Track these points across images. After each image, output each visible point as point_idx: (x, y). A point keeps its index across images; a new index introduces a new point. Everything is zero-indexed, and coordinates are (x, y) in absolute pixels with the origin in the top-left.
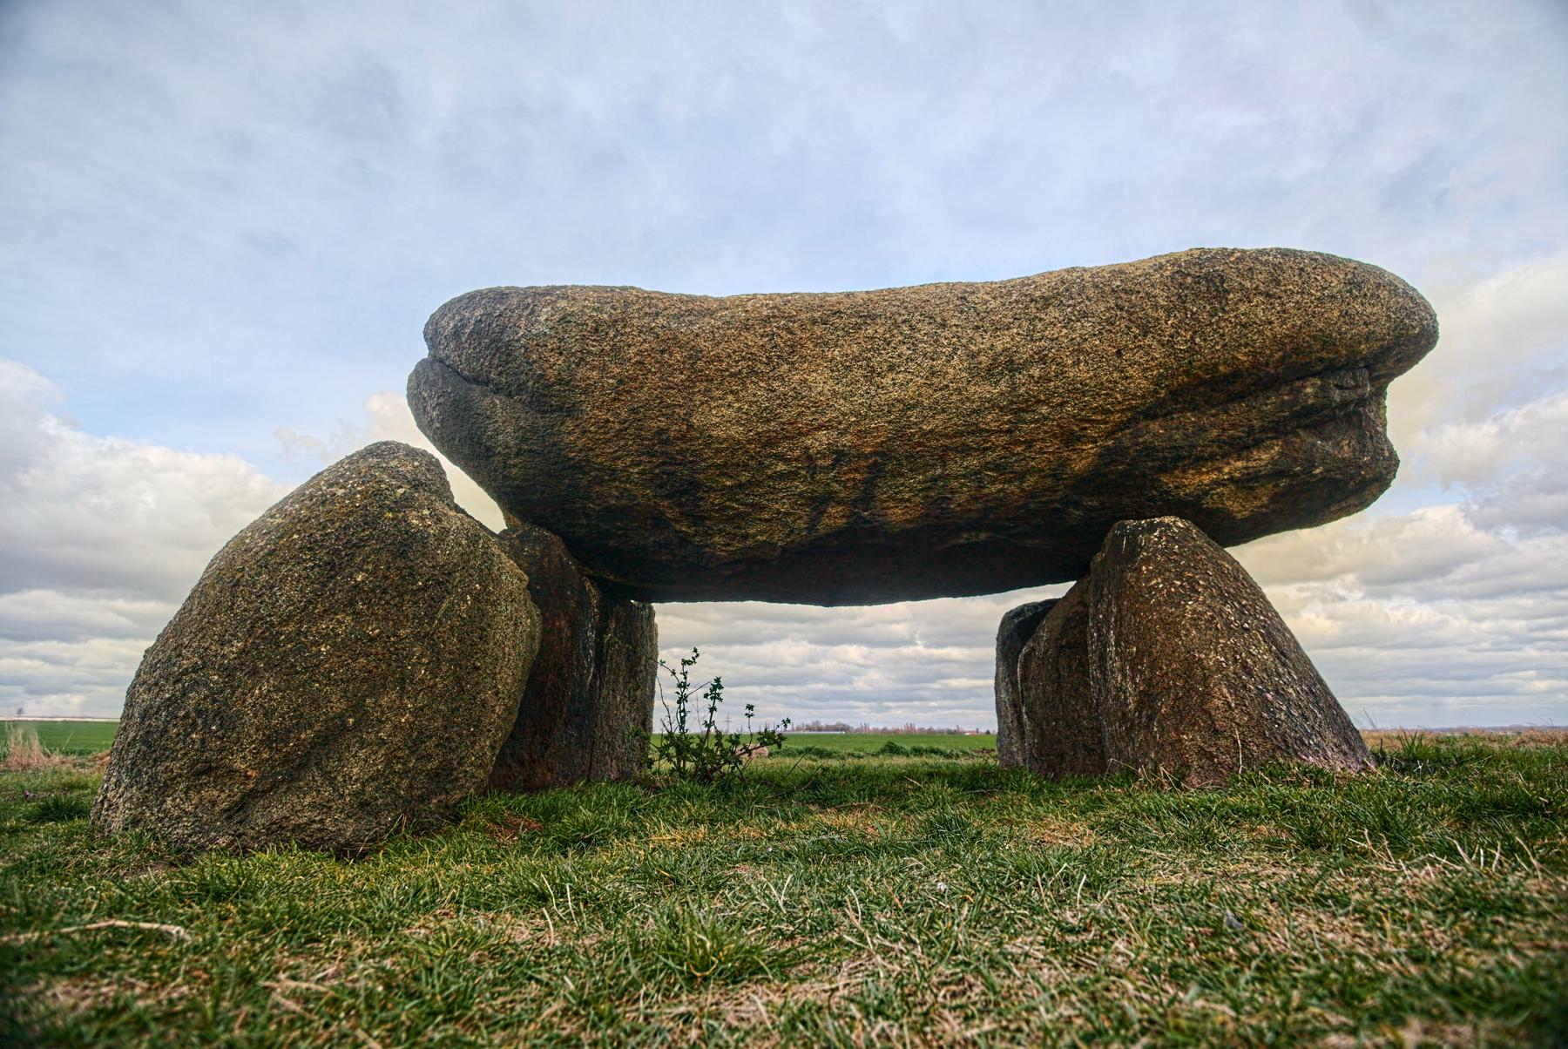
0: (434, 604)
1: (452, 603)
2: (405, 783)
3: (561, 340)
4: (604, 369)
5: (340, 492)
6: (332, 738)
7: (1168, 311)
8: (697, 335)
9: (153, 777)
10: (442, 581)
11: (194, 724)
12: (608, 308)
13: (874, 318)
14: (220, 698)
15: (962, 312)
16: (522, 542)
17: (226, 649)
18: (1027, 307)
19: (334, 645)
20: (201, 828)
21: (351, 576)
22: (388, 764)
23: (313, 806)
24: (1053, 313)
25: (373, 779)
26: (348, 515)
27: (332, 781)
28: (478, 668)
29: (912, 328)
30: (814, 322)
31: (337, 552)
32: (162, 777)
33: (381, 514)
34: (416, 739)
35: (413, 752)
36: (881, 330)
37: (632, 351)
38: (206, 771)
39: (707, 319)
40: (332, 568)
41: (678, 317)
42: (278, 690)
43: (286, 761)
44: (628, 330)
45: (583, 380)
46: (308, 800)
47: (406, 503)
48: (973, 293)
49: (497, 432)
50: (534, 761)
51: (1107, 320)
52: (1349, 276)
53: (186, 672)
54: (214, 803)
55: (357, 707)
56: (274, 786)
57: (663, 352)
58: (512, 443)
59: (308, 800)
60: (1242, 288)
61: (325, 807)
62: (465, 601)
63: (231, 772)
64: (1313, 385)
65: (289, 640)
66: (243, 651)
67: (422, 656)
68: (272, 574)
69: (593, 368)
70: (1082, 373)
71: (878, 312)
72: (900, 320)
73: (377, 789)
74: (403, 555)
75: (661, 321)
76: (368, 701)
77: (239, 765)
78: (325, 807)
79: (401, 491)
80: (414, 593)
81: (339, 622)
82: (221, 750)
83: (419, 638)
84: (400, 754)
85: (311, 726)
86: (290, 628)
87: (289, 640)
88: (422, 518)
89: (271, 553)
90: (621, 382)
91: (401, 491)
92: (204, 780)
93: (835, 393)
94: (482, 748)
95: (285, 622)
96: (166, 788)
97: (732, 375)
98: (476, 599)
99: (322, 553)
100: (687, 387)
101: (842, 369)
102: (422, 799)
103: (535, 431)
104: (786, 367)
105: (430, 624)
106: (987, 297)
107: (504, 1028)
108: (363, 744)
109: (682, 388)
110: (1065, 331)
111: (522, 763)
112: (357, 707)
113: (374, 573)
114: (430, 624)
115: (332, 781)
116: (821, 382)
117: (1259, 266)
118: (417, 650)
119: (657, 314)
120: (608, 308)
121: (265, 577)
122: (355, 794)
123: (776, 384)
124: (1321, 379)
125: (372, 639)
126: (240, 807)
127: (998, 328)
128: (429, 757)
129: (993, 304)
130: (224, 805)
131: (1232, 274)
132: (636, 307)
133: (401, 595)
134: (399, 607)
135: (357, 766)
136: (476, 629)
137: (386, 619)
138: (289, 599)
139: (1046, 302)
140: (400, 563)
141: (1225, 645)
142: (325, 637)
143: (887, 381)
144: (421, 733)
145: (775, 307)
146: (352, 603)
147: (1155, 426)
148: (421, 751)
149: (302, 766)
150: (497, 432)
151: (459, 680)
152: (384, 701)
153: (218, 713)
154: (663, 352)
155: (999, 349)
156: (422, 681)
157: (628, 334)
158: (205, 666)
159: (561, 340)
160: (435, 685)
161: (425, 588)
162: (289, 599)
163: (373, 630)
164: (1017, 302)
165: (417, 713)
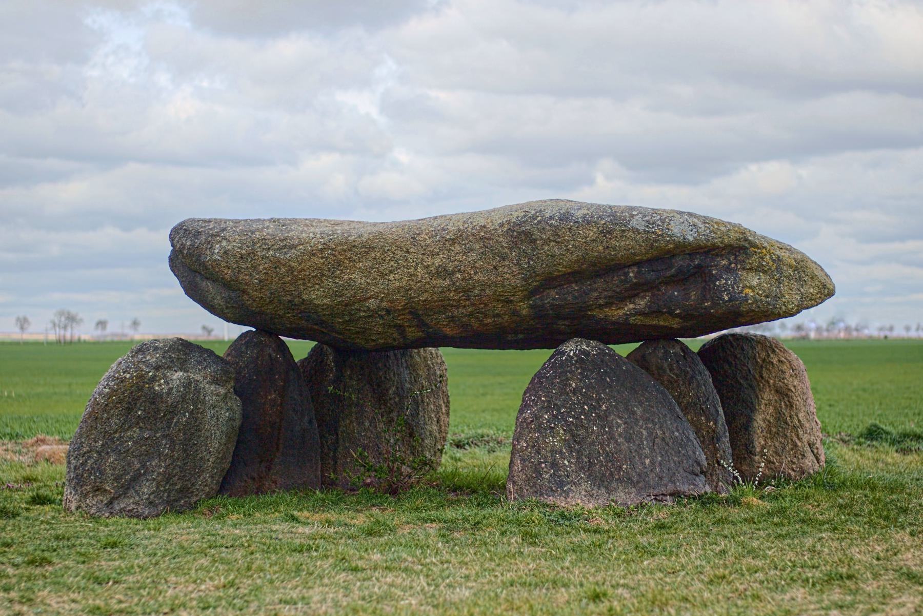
0: (170, 421)
1: (179, 419)
2: (166, 494)
3: (227, 262)
4: (251, 275)
5: (128, 376)
6: (136, 478)
7: (511, 249)
8: (289, 260)
9: (82, 491)
10: (173, 410)
11: (91, 473)
12: (245, 247)
13: (373, 248)
14: (98, 463)
15: (414, 245)
16: (247, 348)
17: (97, 445)
18: (444, 244)
19: (133, 442)
20: (99, 510)
21: (136, 412)
22: (158, 487)
23: (133, 503)
24: (457, 248)
25: (152, 493)
26: (132, 387)
27: (138, 494)
28: (196, 444)
29: (393, 253)
30: (345, 251)
31: (130, 403)
32: (85, 492)
33: (144, 386)
34: (168, 478)
35: (167, 483)
36: (378, 255)
37: (261, 268)
38: (98, 490)
39: (293, 251)
40: (129, 410)
41: (280, 249)
42: (116, 460)
43: (122, 487)
44: (256, 258)
45: (242, 280)
46: (131, 501)
47: (154, 379)
48: (419, 234)
49: (213, 298)
50: (261, 478)
51: (482, 253)
52: (600, 229)
53: (85, 453)
54: (102, 501)
55: (144, 465)
56: (120, 496)
57: (275, 268)
58: (222, 304)
59: (131, 501)
60: (542, 239)
61: (137, 504)
62: (185, 416)
63: (106, 490)
64: (633, 272)
65: (118, 440)
66: (102, 445)
67: (166, 444)
68: (108, 413)
69: (246, 275)
70: (480, 277)
71: (375, 245)
72: (386, 249)
73: (155, 497)
74: (154, 403)
75: (271, 253)
76: (148, 463)
77: (108, 488)
78: (137, 504)
79: (151, 374)
80: (161, 418)
81: (135, 432)
82: (101, 483)
83: (164, 436)
84: (162, 483)
85: (129, 473)
86: (117, 435)
87: (118, 440)
88: (160, 385)
89: (107, 405)
90: (260, 281)
91: (151, 374)
92: (97, 493)
93: (368, 284)
94: (205, 478)
95: (115, 432)
96: (86, 496)
97: (313, 277)
98: (191, 413)
99: (124, 404)
100: (294, 281)
101: (367, 271)
102: (176, 501)
103: (231, 298)
104: (338, 272)
105: (168, 430)
106: (426, 237)
107: (260, 610)
108: (148, 480)
109: (290, 282)
110: (464, 257)
111: (254, 479)
112: (144, 465)
113: (144, 410)
114: (168, 430)
115: (138, 494)
116: (359, 279)
117: (547, 227)
118: (164, 442)
119: (269, 249)
120: (245, 247)
121: (106, 415)
122: (147, 499)
123: (337, 280)
124: (639, 267)
125: (147, 439)
126: (111, 502)
127: (434, 254)
128: (176, 484)
129: (429, 242)
130: (105, 502)
131: (536, 232)
132: (258, 245)
133: (155, 420)
134: (155, 424)
135: (146, 489)
136: (194, 428)
137: (151, 430)
138: (116, 423)
139: (453, 241)
140: (153, 407)
141: (531, 437)
142: (131, 438)
143: (391, 277)
144: (169, 475)
145: (324, 244)
146: (138, 423)
147: (553, 293)
148: (171, 481)
149: (128, 489)
150: (213, 298)
151: (185, 451)
152: (154, 464)
153: (98, 468)
154: (275, 268)
155: (437, 264)
156: (167, 454)
157: (257, 260)
158: (91, 451)
159: (227, 262)
160: (174, 455)
161: (165, 415)
162: (116, 423)
163: (146, 435)
164: (439, 241)
165: (167, 467)
